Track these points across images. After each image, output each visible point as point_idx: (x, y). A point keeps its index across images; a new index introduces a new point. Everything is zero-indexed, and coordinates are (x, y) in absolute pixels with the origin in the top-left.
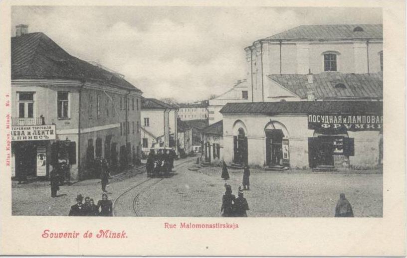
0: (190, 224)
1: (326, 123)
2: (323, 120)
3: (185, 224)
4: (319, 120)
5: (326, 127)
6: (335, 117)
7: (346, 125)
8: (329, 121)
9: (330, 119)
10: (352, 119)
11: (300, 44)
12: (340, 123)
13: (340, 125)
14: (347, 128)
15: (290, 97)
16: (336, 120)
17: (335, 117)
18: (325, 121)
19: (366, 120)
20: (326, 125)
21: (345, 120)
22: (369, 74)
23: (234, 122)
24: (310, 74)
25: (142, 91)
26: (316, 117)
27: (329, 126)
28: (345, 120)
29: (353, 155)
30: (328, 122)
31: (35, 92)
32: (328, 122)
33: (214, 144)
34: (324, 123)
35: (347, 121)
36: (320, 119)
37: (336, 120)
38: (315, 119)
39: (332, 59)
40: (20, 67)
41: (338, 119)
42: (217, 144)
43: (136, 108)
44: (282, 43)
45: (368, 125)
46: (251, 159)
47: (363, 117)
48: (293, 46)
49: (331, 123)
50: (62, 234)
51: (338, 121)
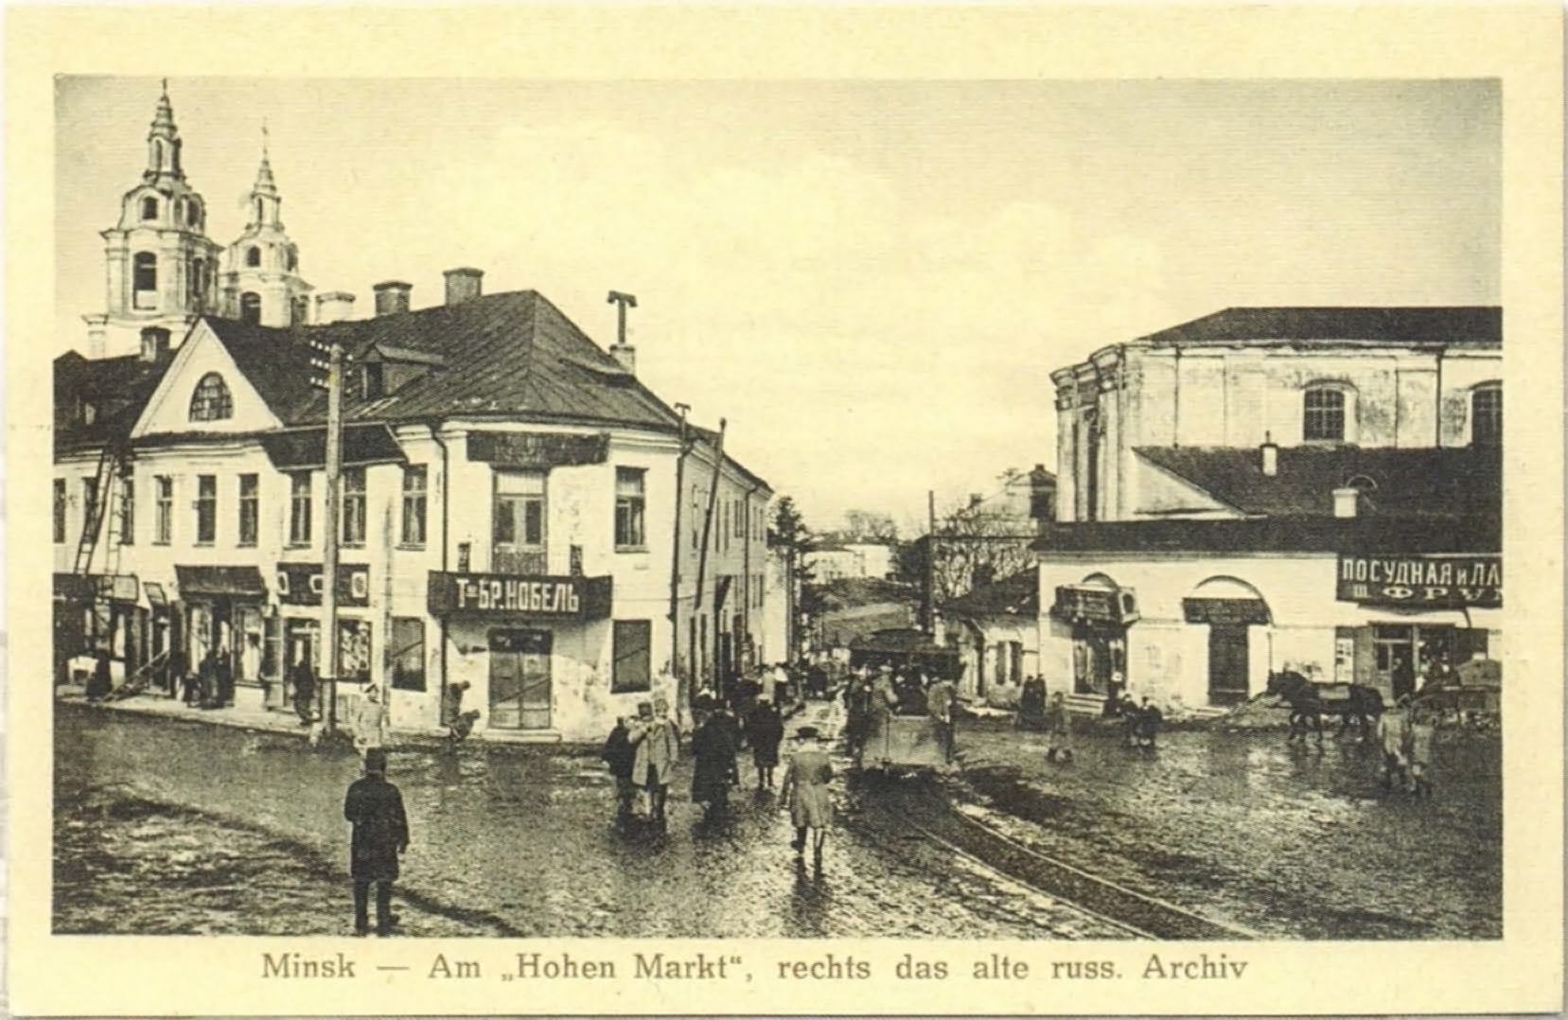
0: (995, 957)
1: (1399, 585)
3: (658, 957)
4: (1376, 575)
6: (1432, 566)
7: (1465, 592)
11: (151, 150)
12: (1445, 585)
13: (1444, 592)
14: (1469, 597)
16: (1432, 575)
17: (1432, 566)
21: (1462, 576)
25: (771, 486)
26: (1369, 566)
28: (1462, 576)
29: (431, 573)
30: (1405, 581)
32: (1405, 581)
34: (1391, 585)
35: (1470, 577)
37: (1432, 575)
40: (485, 351)
43: (117, 524)
48: (1496, 362)
49: (1417, 585)
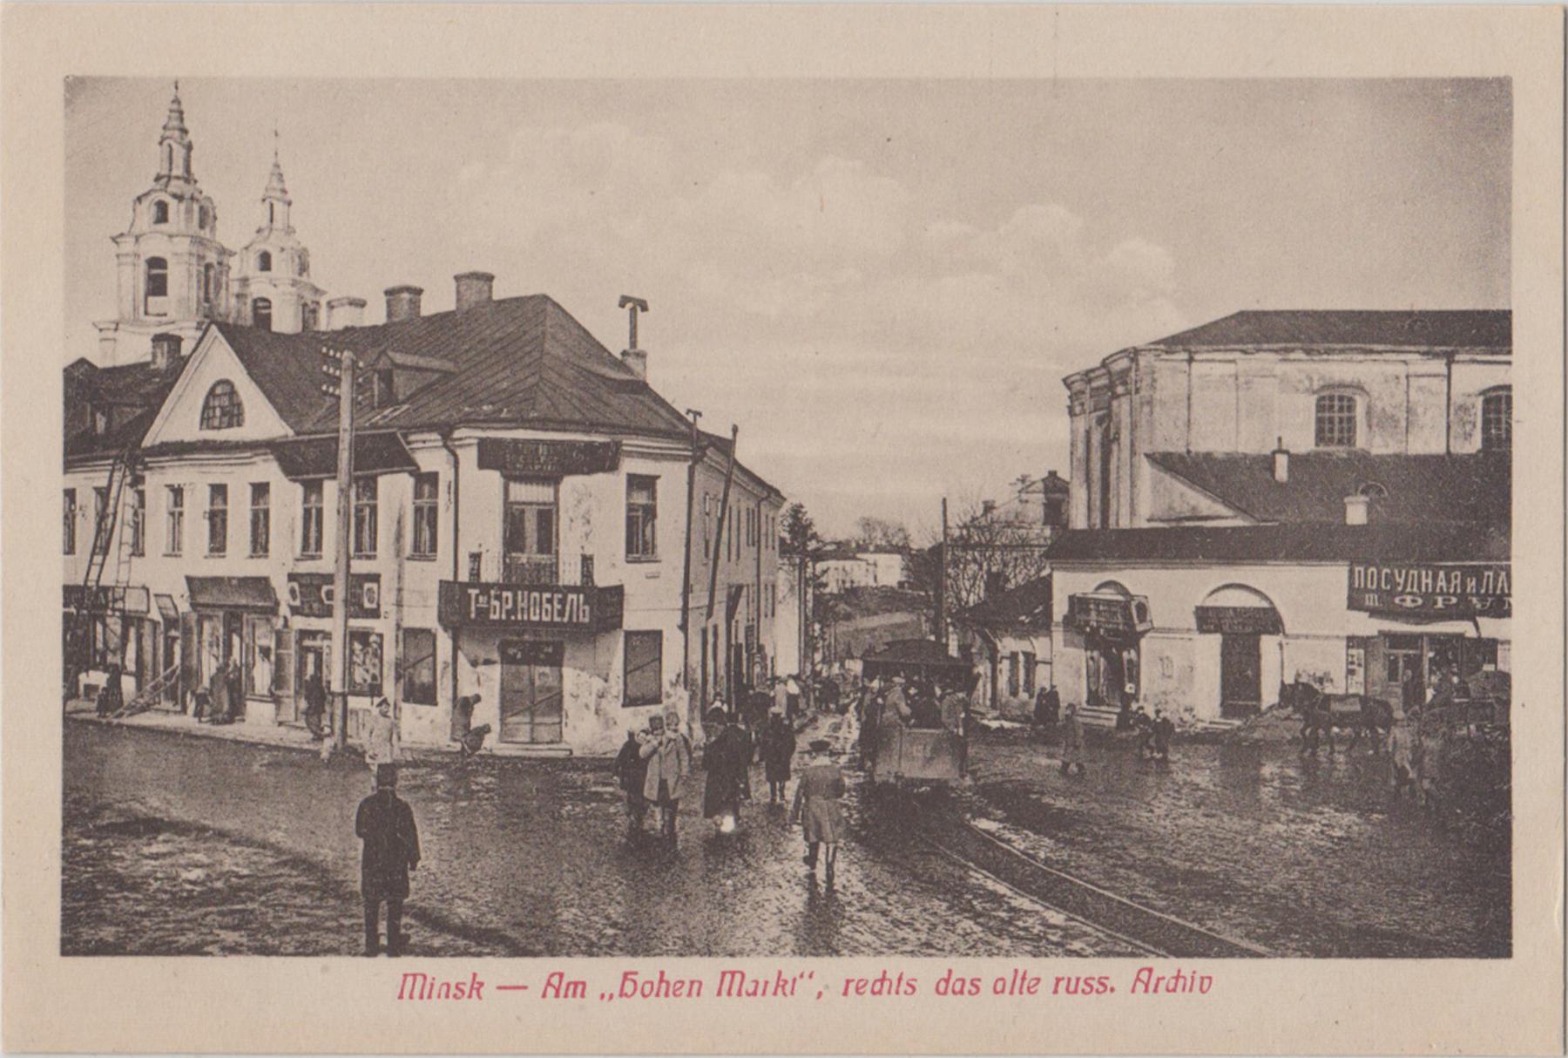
1: (1410, 594)
2: (1401, 581)
5: (1408, 603)
6: (1442, 574)
7: (1475, 600)
8: (1419, 587)
9: (1424, 581)
10: (1496, 580)
12: (1454, 594)
15: (1226, 518)
16: (1442, 583)
17: (1442, 574)
18: (1405, 587)
19: (1366, 575)
20: (1409, 598)
21: (1471, 584)
22: (1189, 452)
23: (1098, 583)
24: (1280, 451)
27: (1420, 601)
31: (658, 477)
32: (1415, 590)
33: (1013, 657)
34: (1402, 593)
35: (1479, 584)
36: (1390, 579)
37: (1442, 583)
38: (1370, 576)
39: (1341, 409)
41: (1449, 581)
42: (1026, 654)
43: (128, 535)
44: (1197, 357)
45: (1440, 599)
46: (350, 699)
47: (1411, 572)
50: (873, 993)
51: (1448, 588)
